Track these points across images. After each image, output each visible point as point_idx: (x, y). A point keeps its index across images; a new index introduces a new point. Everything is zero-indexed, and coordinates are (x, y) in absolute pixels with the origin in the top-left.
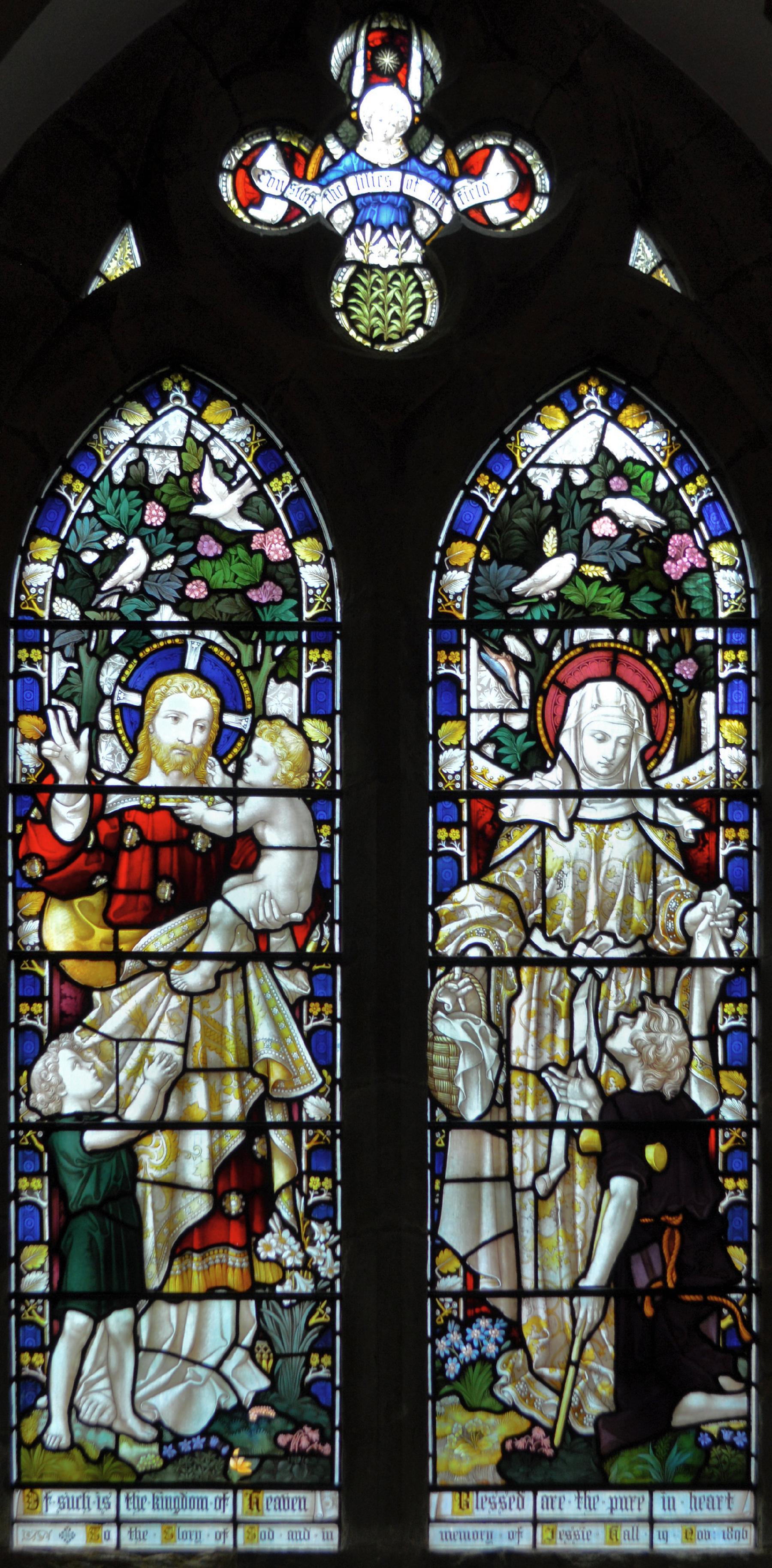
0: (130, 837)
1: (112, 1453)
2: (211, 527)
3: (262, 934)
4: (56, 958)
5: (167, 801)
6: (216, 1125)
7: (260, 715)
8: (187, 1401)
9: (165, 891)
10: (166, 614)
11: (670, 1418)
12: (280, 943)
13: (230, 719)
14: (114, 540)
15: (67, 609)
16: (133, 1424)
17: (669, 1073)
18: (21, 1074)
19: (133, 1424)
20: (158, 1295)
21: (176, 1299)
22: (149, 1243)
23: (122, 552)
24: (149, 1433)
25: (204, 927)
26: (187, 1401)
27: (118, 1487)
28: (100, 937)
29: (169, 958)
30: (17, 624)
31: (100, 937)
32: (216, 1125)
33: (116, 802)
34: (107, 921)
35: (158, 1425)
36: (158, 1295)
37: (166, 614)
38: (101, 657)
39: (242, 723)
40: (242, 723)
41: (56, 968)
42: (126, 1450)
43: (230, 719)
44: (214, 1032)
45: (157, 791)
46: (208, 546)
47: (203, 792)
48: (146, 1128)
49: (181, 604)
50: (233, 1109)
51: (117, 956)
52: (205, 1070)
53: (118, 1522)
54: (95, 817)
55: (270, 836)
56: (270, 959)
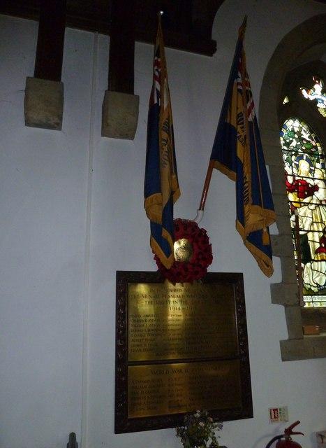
0: (300, 184)
1: (310, 289)
2: (305, 139)
3: (321, 201)
4: (291, 202)
5: (304, 179)
6: (319, 232)
7: (315, 168)
8: (321, 279)
9: (306, 193)
10: (300, 150)
11: (277, 224)
12: (323, 203)
13: (311, 168)
14: (291, 139)
15: (285, 148)
16: (313, 284)
17: (268, 251)
18: (168, 106)
19: (313, 284)
20: (314, 260)
21: (317, 261)
22: (311, 251)
23: (292, 141)
24: (315, 285)
25: (312, 199)
26: (321, 279)
27: (312, 295)
28: (297, 199)
29: (308, 204)
30: (292, 188)
31: (297, 199)
32: (319, 232)
33: (297, 178)
34: (298, 197)
35: (317, 284)
36: (314, 260)
37: (300, 150)
38: (292, 155)
39: (313, 168)
40: (313, 168)
41: (292, 204)
42: (312, 288)
43: (311, 168)
44: (316, 217)
45: (303, 177)
46: (305, 142)
47: (309, 178)
48: (308, 231)
49: (302, 150)
50: (321, 230)
51: (300, 203)
52: (316, 222)
53: (313, 302)
54: (294, 180)
55: (319, 186)
56: (323, 205)
